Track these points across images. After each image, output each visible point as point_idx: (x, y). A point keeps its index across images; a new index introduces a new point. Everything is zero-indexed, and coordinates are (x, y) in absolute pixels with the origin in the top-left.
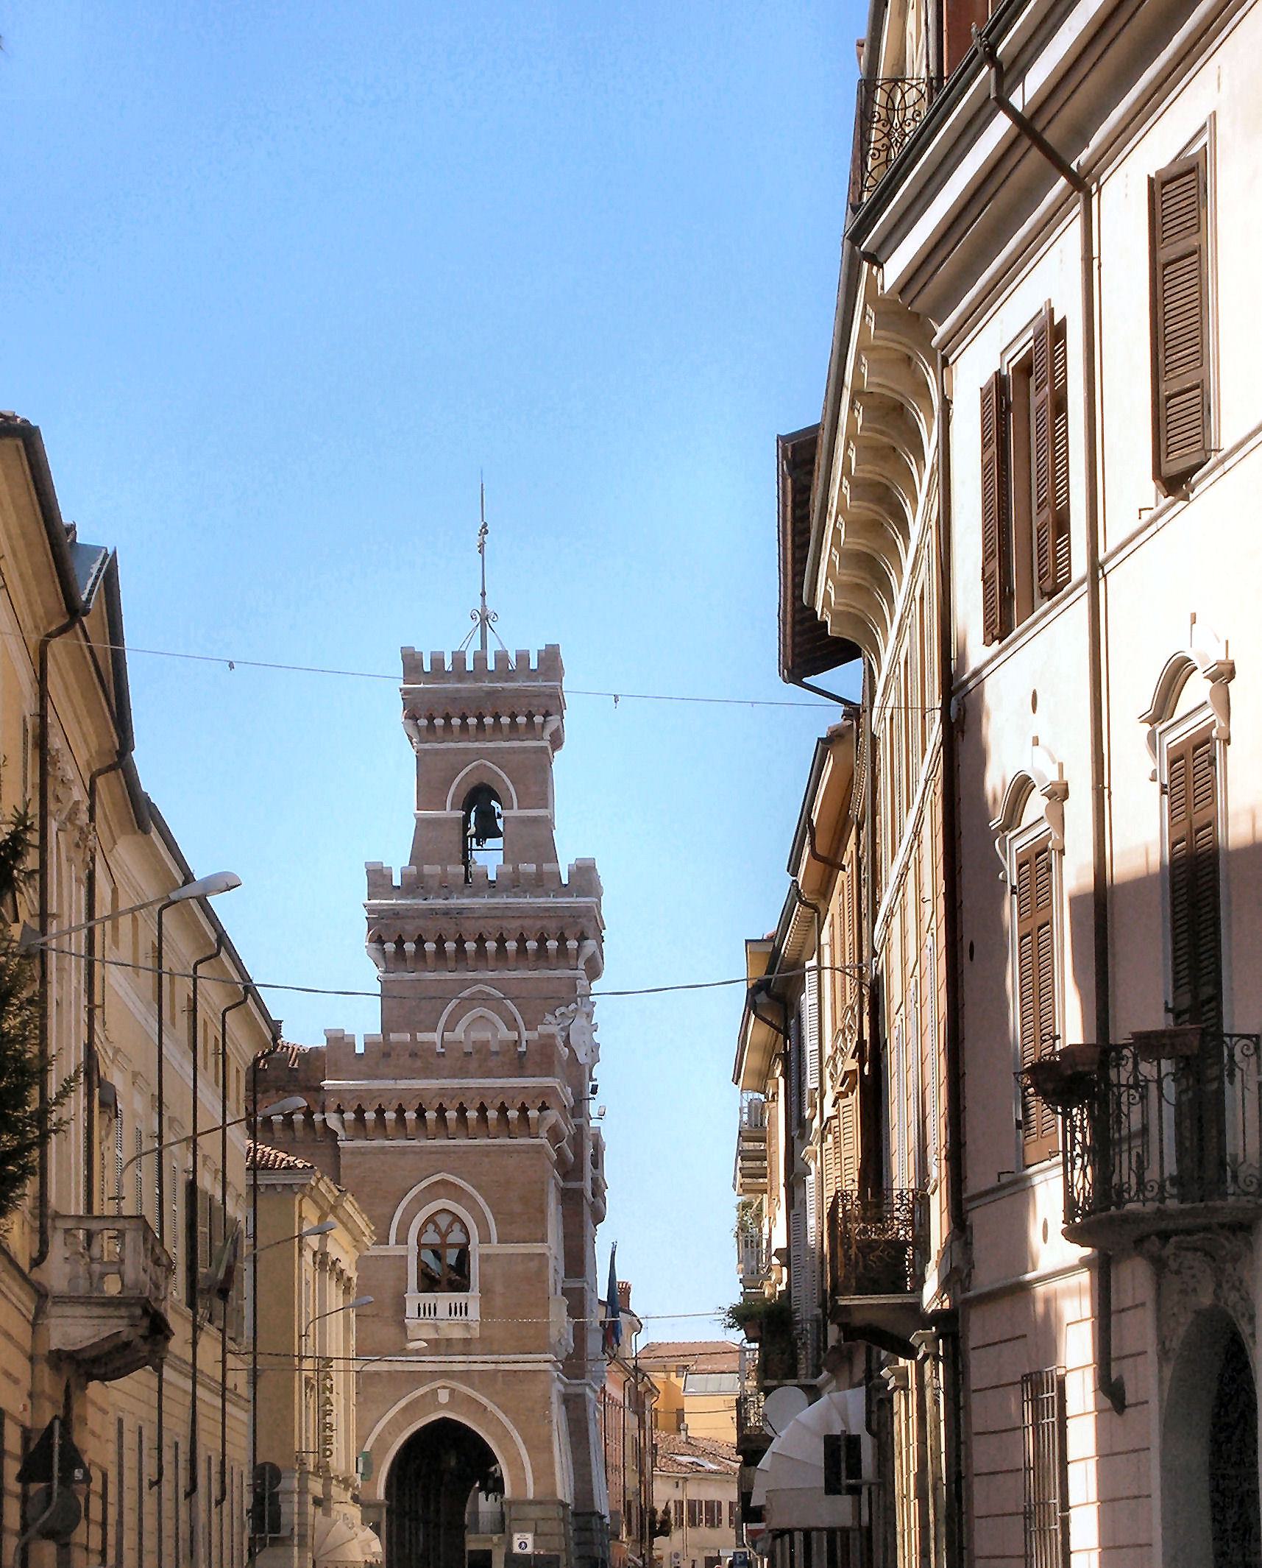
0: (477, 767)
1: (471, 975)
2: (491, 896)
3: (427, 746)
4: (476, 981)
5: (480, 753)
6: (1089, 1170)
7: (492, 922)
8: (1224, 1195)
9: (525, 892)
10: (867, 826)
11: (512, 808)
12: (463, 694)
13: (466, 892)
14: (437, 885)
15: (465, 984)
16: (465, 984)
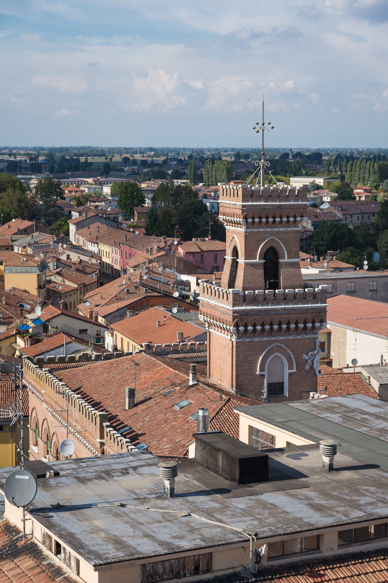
0: (270, 240)
1: (273, 338)
2: (285, 304)
3: (249, 230)
4: (275, 341)
5: (271, 233)
6: (187, 475)
7: (285, 316)
8: (145, 203)
9: (299, 302)
10: (361, 167)
11: (284, 258)
12: (267, 207)
13: (275, 302)
14: (262, 299)
15: (270, 343)
16: (270, 343)
